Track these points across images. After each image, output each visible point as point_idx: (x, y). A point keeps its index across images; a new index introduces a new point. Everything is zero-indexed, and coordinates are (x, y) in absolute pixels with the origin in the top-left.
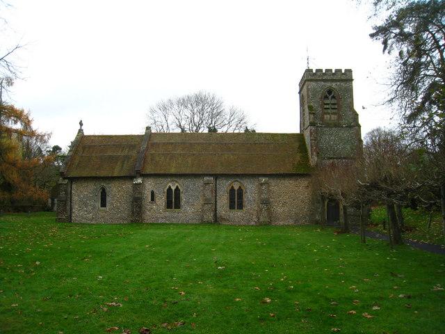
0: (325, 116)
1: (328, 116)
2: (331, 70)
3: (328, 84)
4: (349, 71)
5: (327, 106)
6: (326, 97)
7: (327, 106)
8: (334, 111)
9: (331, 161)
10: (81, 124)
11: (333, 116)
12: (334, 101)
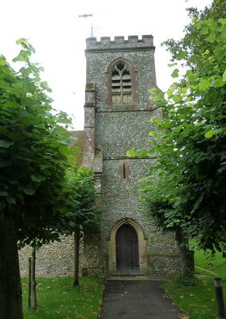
0: (114, 98)
1: (119, 98)
2: (123, 38)
3: (118, 55)
4: (96, 48)
5: (117, 84)
6: (115, 73)
7: (117, 84)
8: (128, 90)
9: (121, 162)
10: (80, 16)
11: (125, 97)
12: (126, 77)
